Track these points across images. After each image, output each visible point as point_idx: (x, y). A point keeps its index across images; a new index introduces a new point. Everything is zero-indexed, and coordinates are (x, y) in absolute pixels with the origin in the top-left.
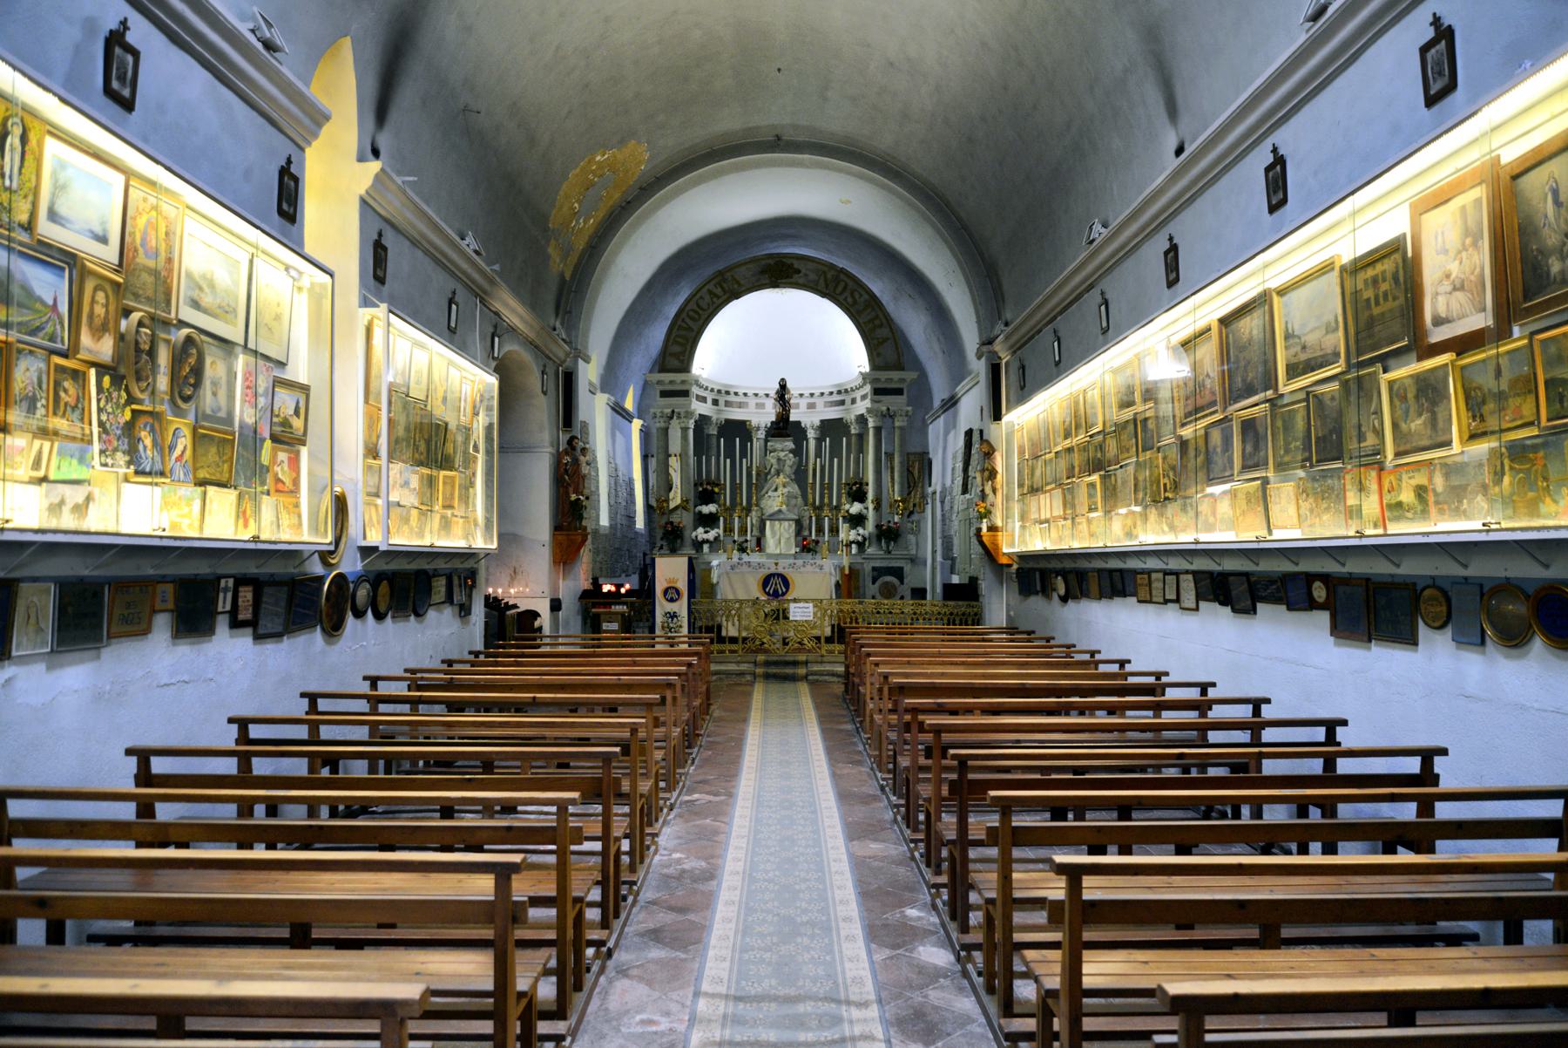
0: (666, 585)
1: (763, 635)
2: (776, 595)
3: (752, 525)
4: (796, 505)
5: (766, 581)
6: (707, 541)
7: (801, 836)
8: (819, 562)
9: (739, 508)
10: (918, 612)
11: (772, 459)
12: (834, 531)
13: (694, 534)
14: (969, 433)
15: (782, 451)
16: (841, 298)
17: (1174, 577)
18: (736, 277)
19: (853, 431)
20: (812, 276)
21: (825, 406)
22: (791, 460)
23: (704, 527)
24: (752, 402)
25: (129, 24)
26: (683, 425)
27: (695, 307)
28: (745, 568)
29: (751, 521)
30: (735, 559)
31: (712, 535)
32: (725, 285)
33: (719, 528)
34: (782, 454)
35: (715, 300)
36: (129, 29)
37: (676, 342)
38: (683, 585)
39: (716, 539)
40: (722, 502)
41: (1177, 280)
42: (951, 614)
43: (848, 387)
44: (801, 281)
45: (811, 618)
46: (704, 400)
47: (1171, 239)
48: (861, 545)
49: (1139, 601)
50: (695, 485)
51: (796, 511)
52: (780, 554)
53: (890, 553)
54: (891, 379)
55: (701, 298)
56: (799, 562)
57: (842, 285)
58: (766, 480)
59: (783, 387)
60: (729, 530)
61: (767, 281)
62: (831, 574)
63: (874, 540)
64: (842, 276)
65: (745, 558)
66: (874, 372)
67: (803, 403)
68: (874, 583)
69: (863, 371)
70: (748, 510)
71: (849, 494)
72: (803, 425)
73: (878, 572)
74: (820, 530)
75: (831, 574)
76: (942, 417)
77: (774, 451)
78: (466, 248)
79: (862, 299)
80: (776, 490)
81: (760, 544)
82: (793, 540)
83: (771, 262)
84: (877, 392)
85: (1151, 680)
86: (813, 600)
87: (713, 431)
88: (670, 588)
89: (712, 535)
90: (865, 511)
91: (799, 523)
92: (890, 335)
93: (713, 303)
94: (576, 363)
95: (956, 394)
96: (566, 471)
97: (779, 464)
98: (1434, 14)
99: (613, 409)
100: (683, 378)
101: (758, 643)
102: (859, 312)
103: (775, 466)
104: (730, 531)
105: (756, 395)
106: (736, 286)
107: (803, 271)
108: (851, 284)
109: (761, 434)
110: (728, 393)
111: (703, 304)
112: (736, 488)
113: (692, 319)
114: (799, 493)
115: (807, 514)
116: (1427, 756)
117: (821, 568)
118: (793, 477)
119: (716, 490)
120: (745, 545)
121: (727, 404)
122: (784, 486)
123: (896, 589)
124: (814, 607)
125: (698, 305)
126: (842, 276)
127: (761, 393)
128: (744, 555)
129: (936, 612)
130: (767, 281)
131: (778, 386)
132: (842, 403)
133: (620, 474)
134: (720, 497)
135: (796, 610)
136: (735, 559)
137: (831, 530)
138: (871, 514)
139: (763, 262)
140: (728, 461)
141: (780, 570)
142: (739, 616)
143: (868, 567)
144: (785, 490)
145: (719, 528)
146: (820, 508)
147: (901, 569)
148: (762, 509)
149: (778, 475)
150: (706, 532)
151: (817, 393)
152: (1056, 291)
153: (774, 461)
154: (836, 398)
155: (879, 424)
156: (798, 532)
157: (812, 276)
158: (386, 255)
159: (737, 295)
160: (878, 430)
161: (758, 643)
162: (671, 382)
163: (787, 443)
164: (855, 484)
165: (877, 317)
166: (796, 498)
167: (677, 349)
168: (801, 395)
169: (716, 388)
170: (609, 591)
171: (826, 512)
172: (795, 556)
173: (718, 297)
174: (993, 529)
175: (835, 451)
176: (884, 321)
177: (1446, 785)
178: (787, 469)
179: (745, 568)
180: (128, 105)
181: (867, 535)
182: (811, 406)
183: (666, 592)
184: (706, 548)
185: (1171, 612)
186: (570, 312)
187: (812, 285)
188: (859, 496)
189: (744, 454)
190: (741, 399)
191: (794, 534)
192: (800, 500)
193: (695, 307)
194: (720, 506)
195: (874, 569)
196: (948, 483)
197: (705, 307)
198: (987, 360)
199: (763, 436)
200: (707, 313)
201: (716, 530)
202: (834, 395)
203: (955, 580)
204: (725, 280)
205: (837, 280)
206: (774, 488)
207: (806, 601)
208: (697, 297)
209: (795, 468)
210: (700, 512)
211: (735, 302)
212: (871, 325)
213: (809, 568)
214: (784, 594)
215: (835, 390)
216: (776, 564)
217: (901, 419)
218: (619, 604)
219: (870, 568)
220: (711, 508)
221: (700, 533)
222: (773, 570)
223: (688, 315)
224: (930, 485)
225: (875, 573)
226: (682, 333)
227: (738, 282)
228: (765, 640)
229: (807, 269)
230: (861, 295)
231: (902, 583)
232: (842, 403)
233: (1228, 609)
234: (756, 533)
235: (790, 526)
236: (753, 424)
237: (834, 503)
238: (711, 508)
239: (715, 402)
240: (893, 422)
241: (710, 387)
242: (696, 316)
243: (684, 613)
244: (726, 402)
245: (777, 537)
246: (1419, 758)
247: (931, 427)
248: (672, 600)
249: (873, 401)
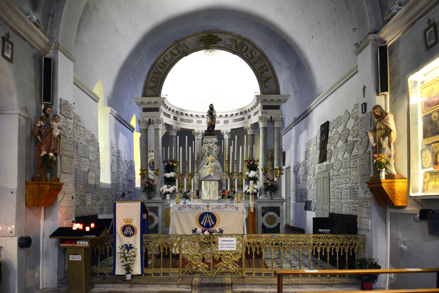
0: (124, 224)
1: (198, 262)
2: (207, 226)
3: (194, 184)
4: (218, 173)
5: (201, 217)
6: (169, 193)
8: (235, 204)
9: (187, 175)
10: (317, 243)
11: (205, 147)
12: (240, 187)
13: (161, 189)
15: (211, 143)
16: (245, 55)
18: (186, 43)
19: (249, 133)
20: (228, 42)
21: (234, 122)
22: (215, 148)
23: (167, 185)
24: (195, 120)
25: (10, 35)
26: (155, 127)
27: (163, 61)
28: (187, 209)
29: (195, 180)
30: (182, 203)
31: (171, 189)
32: (179, 49)
33: (175, 185)
34: (211, 145)
35: (174, 57)
36: (10, 36)
37: (151, 81)
38: (137, 224)
39: (174, 191)
40: (178, 171)
43: (247, 109)
44: (222, 45)
45: (235, 249)
46: (169, 116)
48: (255, 194)
50: (163, 162)
51: (219, 176)
52: (210, 200)
53: (272, 199)
54: (273, 100)
55: (166, 56)
56: (222, 204)
57: (245, 47)
58: (202, 159)
59: (211, 108)
60: (181, 186)
61: (203, 46)
62: (243, 212)
63: (263, 191)
64: (245, 42)
65: (188, 202)
67: (222, 120)
68: (263, 216)
69: (257, 94)
70: (192, 176)
71: (248, 167)
72: (222, 132)
73: (265, 210)
74: (232, 186)
75: (243, 212)
76: (294, 128)
77: (207, 143)
78: (29, 20)
79: (257, 55)
80: (208, 164)
81: (198, 195)
82: (217, 192)
83: (205, 35)
84: (265, 107)
86: (236, 235)
87: (174, 134)
88: (127, 226)
89: (171, 189)
90: (257, 175)
91: (220, 182)
92: (272, 76)
93: (173, 58)
94: (56, 53)
95: (310, 108)
96: (40, 133)
97: (209, 150)
98: (428, 19)
99: (116, 118)
100: (156, 100)
101: (194, 268)
102: (255, 63)
103: (207, 151)
104: (182, 187)
105: (197, 116)
106: (185, 49)
107: (223, 40)
108: (250, 46)
109: (200, 137)
110: (182, 114)
111: (167, 59)
112: (185, 163)
113: (161, 67)
114: (220, 166)
115: (225, 178)
117: (237, 208)
118: (217, 158)
119: (175, 165)
120: (188, 194)
121: (182, 120)
122: (212, 162)
123: (275, 219)
124: (237, 240)
125: (164, 60)
126: (245, 42)
127: (200, 115)
128: (187, 201)
129: (330, 243)
130: (203, 46)
131: (209, 109)
132: (243, 119)
133: (123, 156)
134: (177, 169)
135: (223, 243)
136: (182, 203)
137: (238, 187)
138: (261, 177)
139: (201, 35)
140: (181, 148)
141: (210, 210)
142: (180, 248)
143: (259, 207)
144: (213, 164)
145: (175, 185)
146: (232, 174)
147: (278, 208)
148: (200, 175)
149: (209, 155)
150: (168, 188)
151: (229, 114)
153: (206, 149)
154: (239, 116)
155: (266, 126)
156: (220, 188)
157: (228, 42)
159: (186, 54)
160: (265, 129)
161: (194, 268)
162: (149, 103)
163: (214, 139)
164: (251, 161)
165: (265, 65)
166: (219, 169)
167: (152, 84)
168: (221, 116)
169: (176, 110)
170: (78, 229)
171: (235, 176)
172: (218, 201)
173: (176, 55)
174: (390, 176)
175: (240, 142)
176: (269, 68)
178: (214, 153)
179: (187, 209)
181: (259, 189)
182: (226, 122)
183: (124, 229)
184: (168, 196)
186: (53, 16)
187: (228, 47)
188: (253, 167)
189: (190, 144)
190: (189, 118)
191: (217, 188)
192: (221, 169)
193: (163, 61)
194: (177, 173)
195: (263, 208)
196: (302, 159)
197: (168, 61)
198: (374, 46)
199: (201, 138)
200: (169, 64)
201: (174, 187)
202: (239, 115)
204: (179, 46)
205: (242, 45)
206: (206, 163)
207: (231, 235)
208: (164, 55)
209: (218, 153)
210: (165, 177)
212: (261, 70)
213: (229, 209)
214: (212, 226)
215: (239, 112)
216: (208, 206)
217: (278, 123)
218: (83, 240)
219: (261, 208)
220: (172, 174)
221: (165, 188)
222: (206, 210)
223: (159, 66)
224: (284, 165)
225: (264, 210)
226: (155, 75)
227: (187, 47)
228: (199, 266)
229: (225, 39)
230: (256, 53)
231: (279, 216)
232: (243, 119)
234: (196, 188)
235: (215, 184)
236: (196, 131)
237: (240, 171)
238: (172, 174)
239: (175, 118)
240: (273, 125)
241: (172, 108)
242: (163, 66)
243: (137, 246)
244: (181, 119)
245: (209, 190)
246: (436, 273)
247: (284, 137)
248: (128, 235)
249: (262, 113)
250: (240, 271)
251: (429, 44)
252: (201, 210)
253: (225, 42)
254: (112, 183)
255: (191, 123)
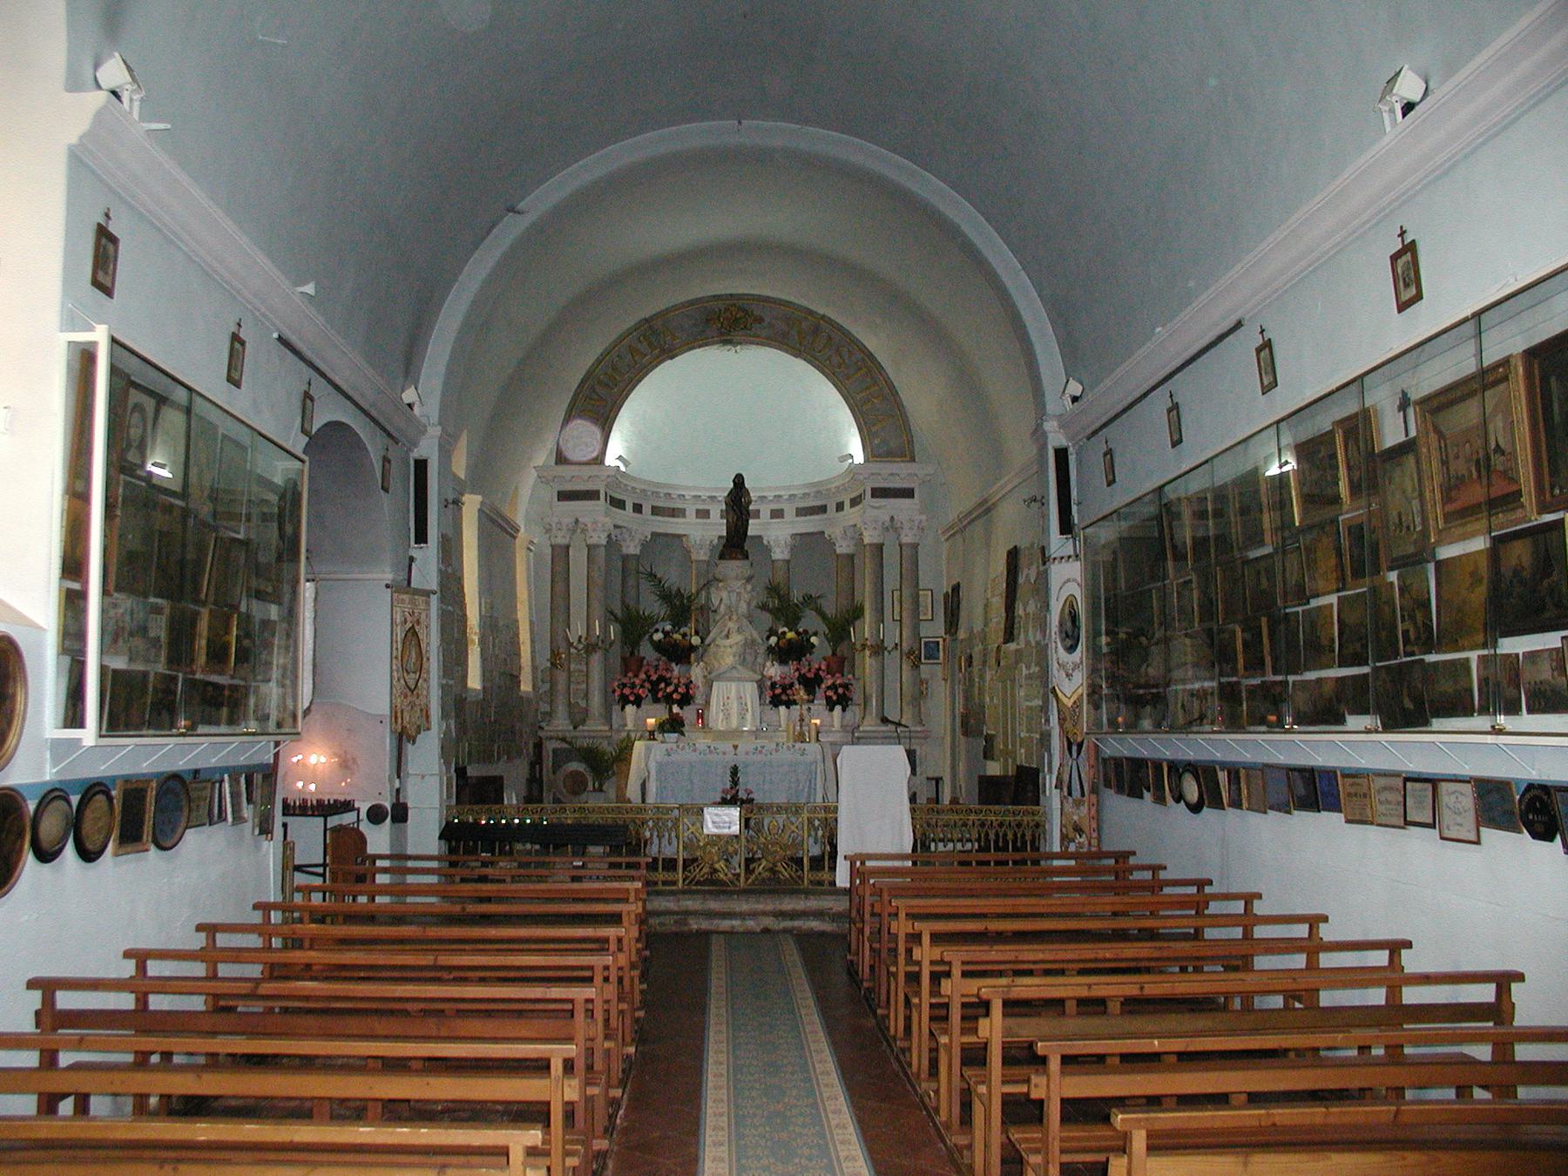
7: (756, 1076)
14: (1013, 555)
17: (1429, 786)
41: (1275, 384)
42: (1001, 825)
47: (1401, 227)
49: (1348, 821)
59: (739, 481)
66: (876, 467)
80: (727, 637)
85: (1193, 890)
107: (767, 320)
116: (1504, 981)
152: (307, 1063)
158: (116, 251)
177: (1522, 1019)
180: (108, 291)
185: (1420, 842)
203: (994, 769)
205: (816, 330)
206: (725, 632)
211: (668, 365)
233: (1336, 818)
250: (799, 877)
251: (1408, 257)
252: (721, 754)
253: (771, 325)
254: (484, 688)
255: (678, 517)
